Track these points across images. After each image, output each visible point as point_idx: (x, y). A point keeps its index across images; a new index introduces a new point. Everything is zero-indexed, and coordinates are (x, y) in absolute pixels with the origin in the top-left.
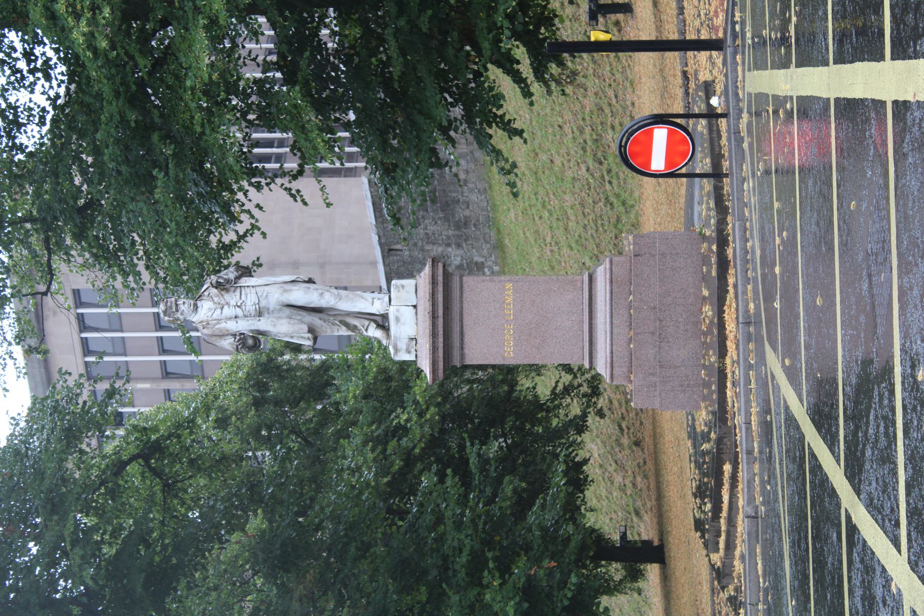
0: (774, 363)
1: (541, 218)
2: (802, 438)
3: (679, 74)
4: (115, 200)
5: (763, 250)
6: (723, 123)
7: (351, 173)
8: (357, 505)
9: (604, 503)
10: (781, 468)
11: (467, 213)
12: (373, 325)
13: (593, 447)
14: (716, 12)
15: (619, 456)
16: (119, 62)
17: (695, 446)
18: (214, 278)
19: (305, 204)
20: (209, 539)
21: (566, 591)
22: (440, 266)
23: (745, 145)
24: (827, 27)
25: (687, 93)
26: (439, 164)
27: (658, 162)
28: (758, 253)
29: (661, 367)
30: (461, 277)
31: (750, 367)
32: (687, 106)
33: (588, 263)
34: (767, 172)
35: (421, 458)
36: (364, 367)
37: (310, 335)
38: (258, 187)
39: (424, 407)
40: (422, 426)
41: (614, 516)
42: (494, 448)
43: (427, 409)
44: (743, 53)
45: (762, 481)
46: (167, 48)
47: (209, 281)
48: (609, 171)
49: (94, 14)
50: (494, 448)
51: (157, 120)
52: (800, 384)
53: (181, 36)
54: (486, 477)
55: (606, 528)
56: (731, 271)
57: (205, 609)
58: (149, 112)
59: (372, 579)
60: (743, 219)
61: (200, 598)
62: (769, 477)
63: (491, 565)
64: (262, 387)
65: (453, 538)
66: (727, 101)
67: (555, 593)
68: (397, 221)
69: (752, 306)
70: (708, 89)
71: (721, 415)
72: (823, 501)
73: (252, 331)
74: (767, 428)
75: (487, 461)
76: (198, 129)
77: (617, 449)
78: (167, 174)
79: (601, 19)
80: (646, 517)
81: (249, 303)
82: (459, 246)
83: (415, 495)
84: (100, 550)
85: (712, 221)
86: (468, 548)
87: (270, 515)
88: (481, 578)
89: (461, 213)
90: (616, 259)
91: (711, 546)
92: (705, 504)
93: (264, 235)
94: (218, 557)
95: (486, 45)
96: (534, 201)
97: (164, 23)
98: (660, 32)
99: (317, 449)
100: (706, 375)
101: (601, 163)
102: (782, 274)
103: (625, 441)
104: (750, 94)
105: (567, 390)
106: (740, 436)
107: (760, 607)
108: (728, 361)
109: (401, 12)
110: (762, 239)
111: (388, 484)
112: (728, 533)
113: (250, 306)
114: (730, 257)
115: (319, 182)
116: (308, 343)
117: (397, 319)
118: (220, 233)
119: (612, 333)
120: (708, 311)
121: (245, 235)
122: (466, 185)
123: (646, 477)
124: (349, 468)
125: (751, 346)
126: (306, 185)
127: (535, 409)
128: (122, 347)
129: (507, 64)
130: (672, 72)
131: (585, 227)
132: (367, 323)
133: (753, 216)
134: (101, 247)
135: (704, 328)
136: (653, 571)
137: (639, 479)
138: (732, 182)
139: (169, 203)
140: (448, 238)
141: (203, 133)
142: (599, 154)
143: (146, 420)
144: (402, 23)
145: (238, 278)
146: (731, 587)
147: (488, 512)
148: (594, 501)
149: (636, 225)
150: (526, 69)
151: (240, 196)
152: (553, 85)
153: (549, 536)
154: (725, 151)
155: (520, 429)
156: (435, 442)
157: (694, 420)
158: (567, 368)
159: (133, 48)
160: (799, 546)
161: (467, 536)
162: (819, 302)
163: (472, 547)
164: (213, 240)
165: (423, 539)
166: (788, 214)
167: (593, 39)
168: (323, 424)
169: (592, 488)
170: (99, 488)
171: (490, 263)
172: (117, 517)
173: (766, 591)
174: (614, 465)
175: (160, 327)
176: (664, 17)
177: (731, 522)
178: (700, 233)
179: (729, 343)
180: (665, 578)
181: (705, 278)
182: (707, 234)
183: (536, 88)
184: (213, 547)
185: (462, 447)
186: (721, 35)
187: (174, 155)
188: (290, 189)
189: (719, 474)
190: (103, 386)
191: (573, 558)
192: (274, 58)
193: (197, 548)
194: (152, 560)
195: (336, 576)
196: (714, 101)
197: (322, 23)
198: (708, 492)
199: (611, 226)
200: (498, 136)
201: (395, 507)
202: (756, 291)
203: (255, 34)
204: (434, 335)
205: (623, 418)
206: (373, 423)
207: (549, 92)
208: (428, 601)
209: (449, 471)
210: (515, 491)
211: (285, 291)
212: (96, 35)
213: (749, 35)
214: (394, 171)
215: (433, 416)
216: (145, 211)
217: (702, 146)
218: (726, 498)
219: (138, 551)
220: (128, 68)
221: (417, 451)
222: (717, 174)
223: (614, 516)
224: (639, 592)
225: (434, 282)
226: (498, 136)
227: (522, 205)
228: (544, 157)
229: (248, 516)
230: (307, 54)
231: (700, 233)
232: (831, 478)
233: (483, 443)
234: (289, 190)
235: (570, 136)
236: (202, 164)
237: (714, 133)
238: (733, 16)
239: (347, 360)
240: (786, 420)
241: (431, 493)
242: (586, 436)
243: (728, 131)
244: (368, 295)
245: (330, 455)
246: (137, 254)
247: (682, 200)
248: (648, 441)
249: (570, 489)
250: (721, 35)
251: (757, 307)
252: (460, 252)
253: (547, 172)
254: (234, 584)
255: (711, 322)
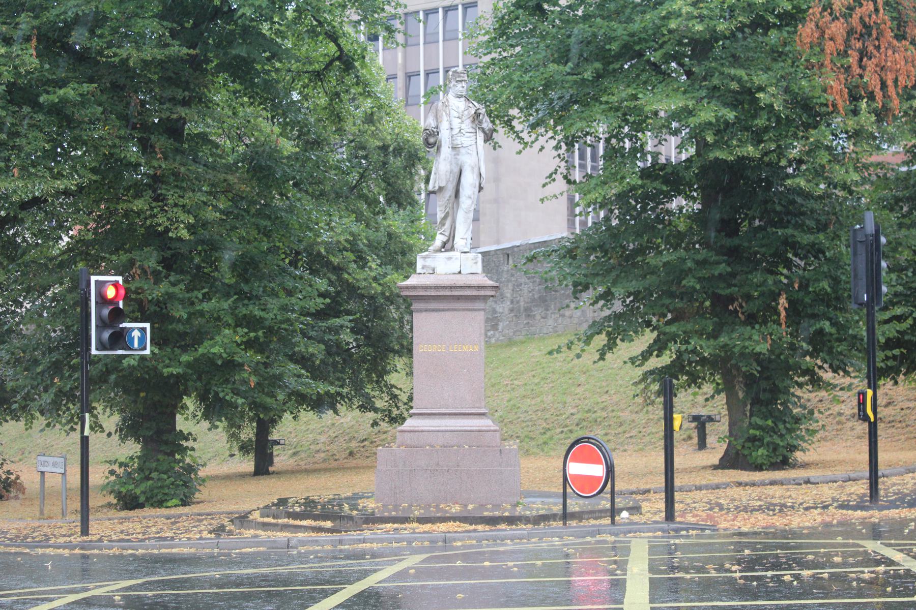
0: (412, 561)
1: (534, 376)
2: (350, 583)
3: (648, 487)
4: (547, 33)
5: (504, 552)
6: (607, 521)
7: (571, 223)
8: (301, 227)
9: (303, 427)
10: (327, 567)
11: (538, 317)
12: (445, 239)
13: (349, 419)
14: (697, 516)
15: (342, 440)
16: (658, 36)
17: (347, 498)
18: (483, 111)
19: (544, 186)
20: (274, 107)
21: (231, 395)
22: (493, 293)
23: (589, 539)
24: (680, 602)
25: (632, 493)
26: (576, 295)
27: (576, 468)
28: (502, 549)
29: (411, 471)
30: (484, 310)
31: (410, 542)
32: (621, 493)
33: (497, 415)
34: (567, 556)
35: (340, 279)
36: (413, 233)
37: (437, 188)
38: (557, 148)
39: (381, 282)
40: (365, 280)
41: (293, 435)
42: (347, 337)
43: (380, 284)
44: (663, 537)
45: (318, 551)
46: (669, 75)
47: (481, 107)
48: (571, 431)
49: (696, 17)
50: (347, 337)
51: (611, 67)
52: (394, 581)
53: (679, 88)
54: (324, 332)
55: (283, 429)
56: (487, 528)
57: (218, 105)
58: (618, 60)
59: (241, 239)
60: (529, 537)
61: (227, 101)
62: (321, 557)
63: (252, 335)
64: (398, 151)
65: (273, 304)
66: (625, 524)
67: (229, 386)
68: (531, 259)
69: (459, 544)
70: (635, 509)
71: (371, 519)
72: (299, 599)
73: (440, 141)
74: (360, 556)
75: (337, 333)
76: (604, 99)
77: (346, 438)
78: (568, 74)
79: (694, 424)
80: (292, 461)
81: (463, 139)
82: (512, 310)
83: (310, 274)
84: (265, 21)
85: (528, 513)
86: (266, 316)
87: (295, 157)
88: (240, 326)
89: (538, 312)
90: (498, 434)
91: (266, 511)
92: (300, 506)
93: (520, 152)
94: (261, 116)
95: (673, 329)
96: (547, 371)
97: (689, 74)
98: (682, 472)
99: (349, 195)
100: (404, 507)
101: (577, 425)
102: (483, 567)
103: (353, 444)
104: (629, 542)
105: (394, 397)
106: (354, 535)
107: (216, 550)
108: (415, 525)
109: (698, 263)
110: (513, 552)
111: (319, 253)
112: (276, 525)
113: (460, 140)
114: (499, 527)
115: (561, 194)
116: (430, 187)
117: (450, 258)
118: (520, 117)
119: (438, 431)
120: (456, 509)
121: (519, 138)
122: (561, 315)
123: (325, 460)
124: (331, 220)
125: (426, 543)
126: (560, 185)
127: (378, 369)
128: (431, 40)
129: (659, 346)
130: (649, 481)
131: (527, 412)
132: (447, 234)
133: (532, 545)
134: (510, 22)
135: (442, 506)
136: (248, 465)
137: (323, 455)
138: (560, 528)
139: (545, 76)
140: (518, 302)
141: (601, 103)
142: (585, 423)
143: (372, 60)
144: (689, 264)
145: (483, 130)
146: (232, 527)
147: (295, 331)
148: (305, 419)
149: (527, 453)
150: (654, 363)
151: (550, 134)
152: (642, 386)
153: (276, 381)
154: (584, 523)
155: (363, 360)
156: (352, 290)
157: (368, 497)
158: (411, 399)
159: (668, 48)
160: (263, 580)
161: (275, 315)
162: (460, 596)
163: (266, 319)
164: (514, 112)
165: (273, 279)
166: (530, 571)
167: (675, 416)
168: (365, 198)
169: (315, 417)
170: (317, 21)
171: (497, 335)
172: (293, 35)
173: (229, 555)
174: (334, 435)
175: (446, 71)
176: (694, 475)
177: (285, 527)
178: (518, 503)
179: (429, 525)
180: (243, 476)
181: (482, 506)
182: (518, 509)
183: (639, 372)
184: (267, 111)
185: (349, 313)
186: (678, 519)
187: (583, 80)
188: (556, 173)
189: (325, 517)
190: (396, 24)
191: (258, 400)
192: (662, 160)
193: (267, 99)
194: (258, 63)
195: (244, 210)
196: (625, 514)
197: (688, 197)
198: (310, 510)
199: (527, 433)
200: (601, 340)
201: (300, 257)
202: (471, 546)
203: (680, 147)
204: (437, 288)
205: (372, 443)
206: (369, 241)
207: (635, 384)
208: (223, 284)
209: (328, 300)
210: (313, 355)
211: (473, 168)
212: (680, 19)
213: (677, 541)
214: (570, 257)
215: (375, 289)
216: (539, 56)
217: (589, 504)
218: (305, 523)
219: (264, 51)
220: (653, 43)
221: (346, 276)
222: (565, 516)
223: (293, 435)
224: (232, 455)
225: (480, 288)
226: (601, 340)
227: (545, 361)
228: (582, 379)
229: (294, 140)
230: (665, 188)
231: (518, 503)
232: (316, 605)
233: (352, 330)
234: (556, 172)
235: (600, 400)
236: (576, 102)
237: (596, 514)
238: (693, 529)
239: (419, 219)
240: (365, 570)
241: (311, 286)
242: (357, 412)
243: (600, 525)
244: (469, 235)
245: (343, 206)
246: (504, 51)
247: (546, 489)
248: (352, 462)
249: (314, 397)
250: (678, 519)
251: (457, 548)
252: (506, 311)
253: (570, 381)
254: (238, 129)
255: (447, 512)
